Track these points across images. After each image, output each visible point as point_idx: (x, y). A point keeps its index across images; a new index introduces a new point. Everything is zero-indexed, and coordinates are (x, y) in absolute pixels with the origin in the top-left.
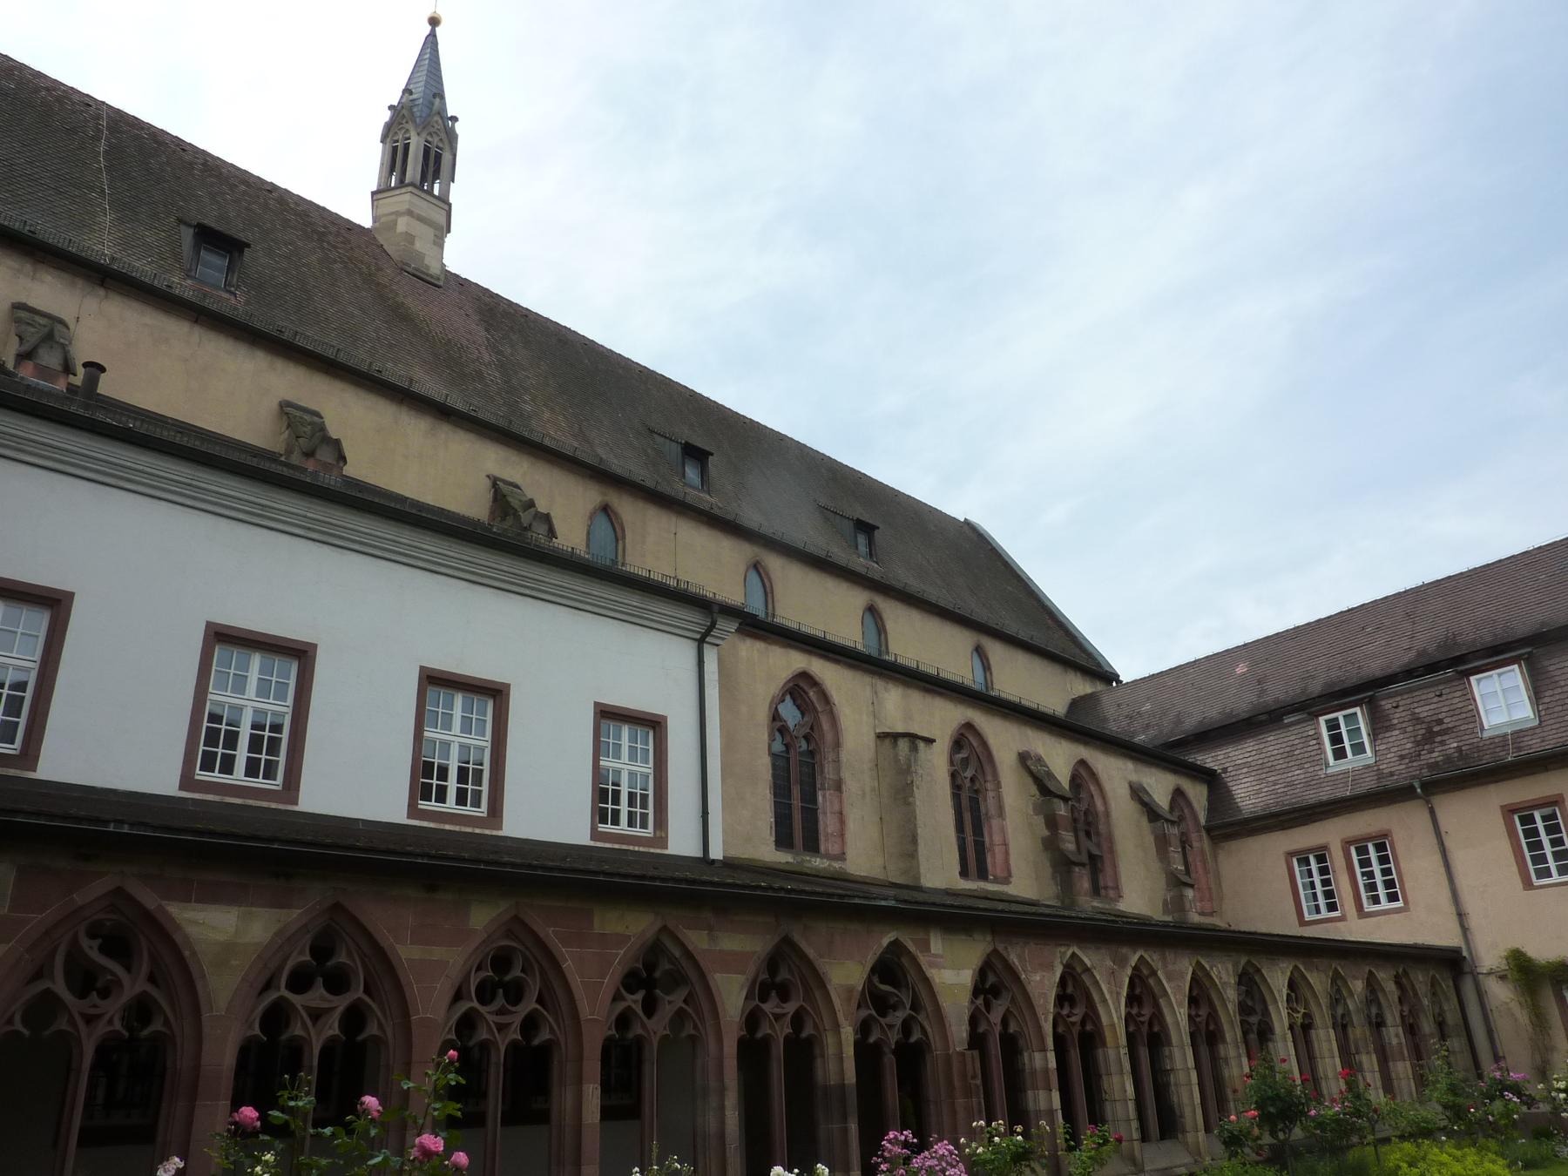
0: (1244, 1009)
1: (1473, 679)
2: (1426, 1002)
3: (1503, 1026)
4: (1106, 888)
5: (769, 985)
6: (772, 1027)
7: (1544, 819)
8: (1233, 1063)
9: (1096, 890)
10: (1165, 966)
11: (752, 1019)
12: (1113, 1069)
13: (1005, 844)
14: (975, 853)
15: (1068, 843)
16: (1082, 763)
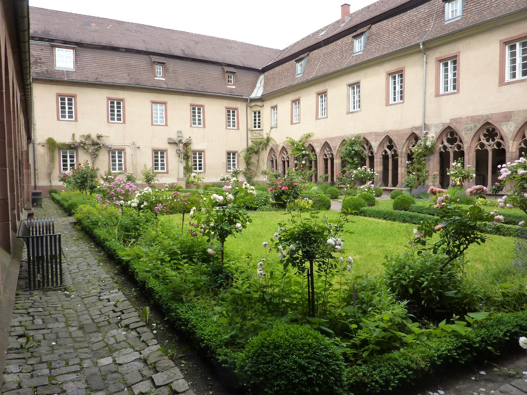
1: (56, 49)
3: (39, 159)
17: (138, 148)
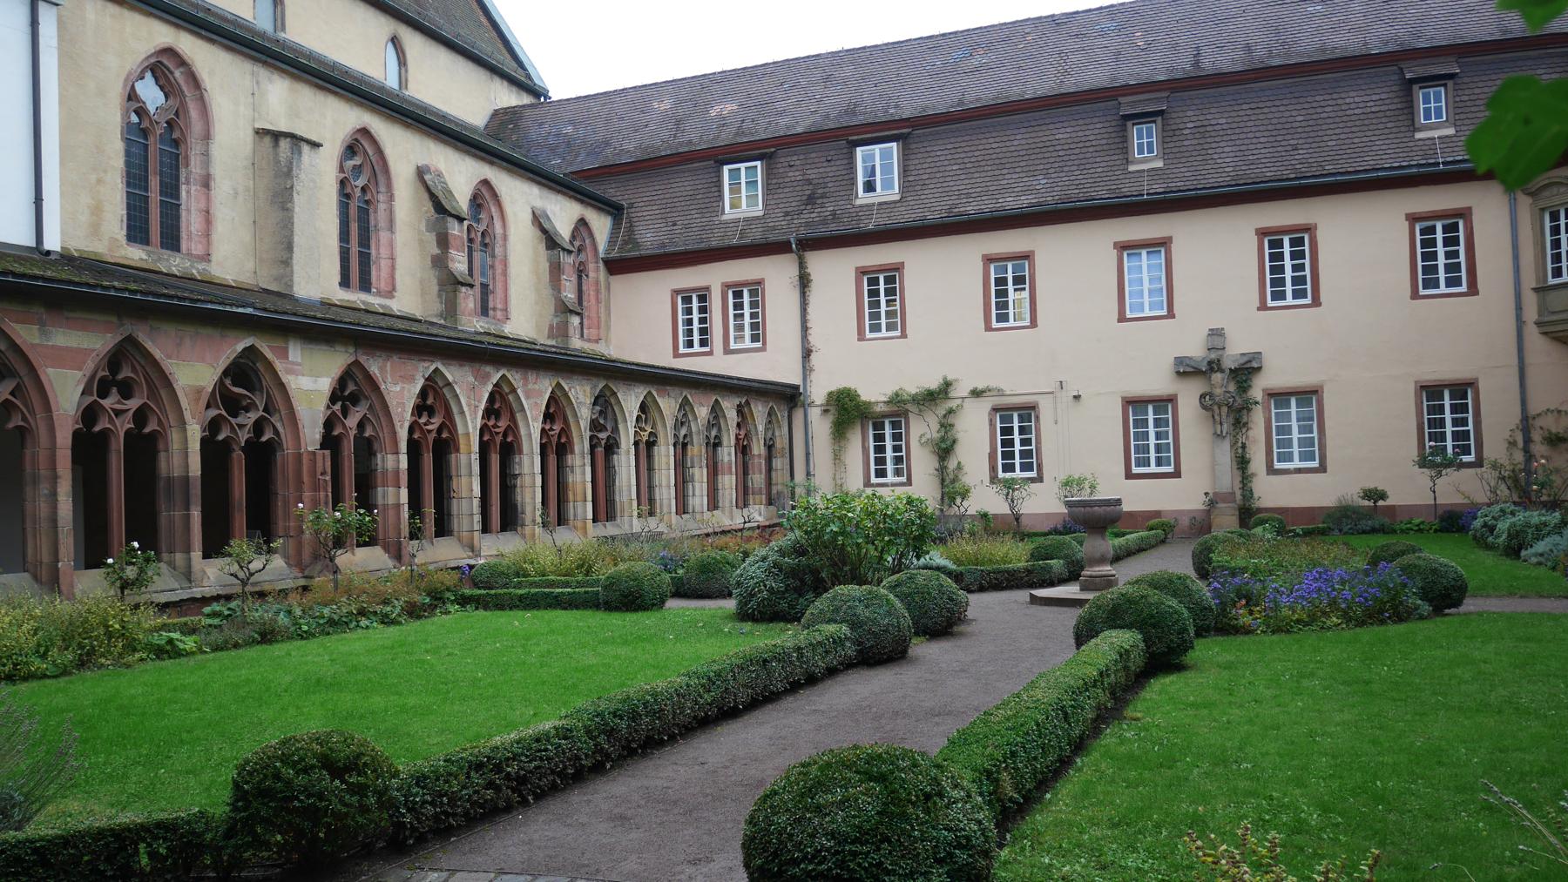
0: (595, 426)
2: (761, 428)
4: (494, 309)
6: (111, 421)
7: (1446, 229)
8: (578, 471)
9: (484, 310)
10: (525, 385)
11: (89, 414)
12: (463, 471)
13: (393, 259)
14: (357, 264)
15: (459, 264)
16: (486, 183)
17: (1077, 397)
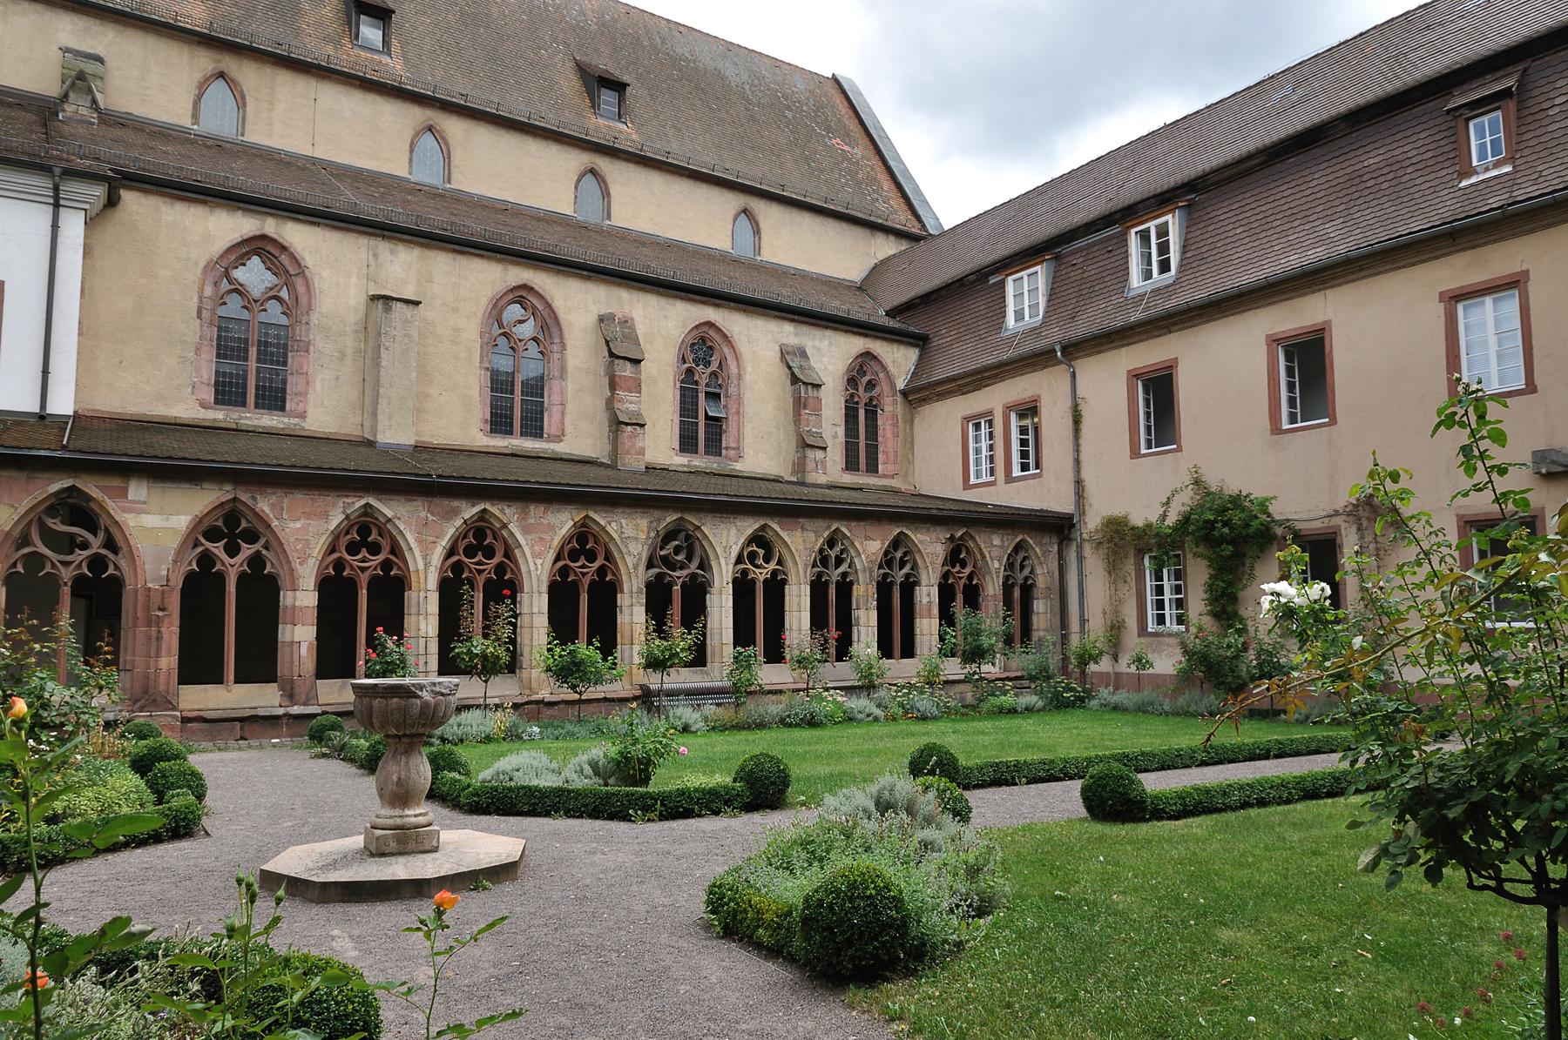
5: (955, 556)
